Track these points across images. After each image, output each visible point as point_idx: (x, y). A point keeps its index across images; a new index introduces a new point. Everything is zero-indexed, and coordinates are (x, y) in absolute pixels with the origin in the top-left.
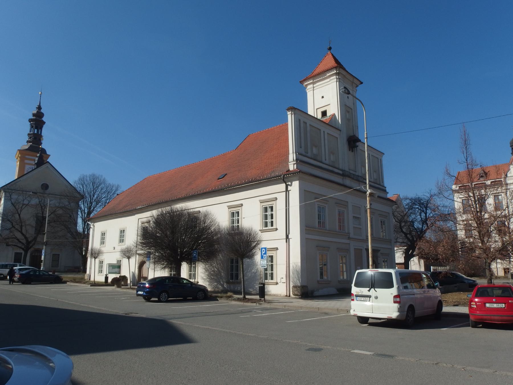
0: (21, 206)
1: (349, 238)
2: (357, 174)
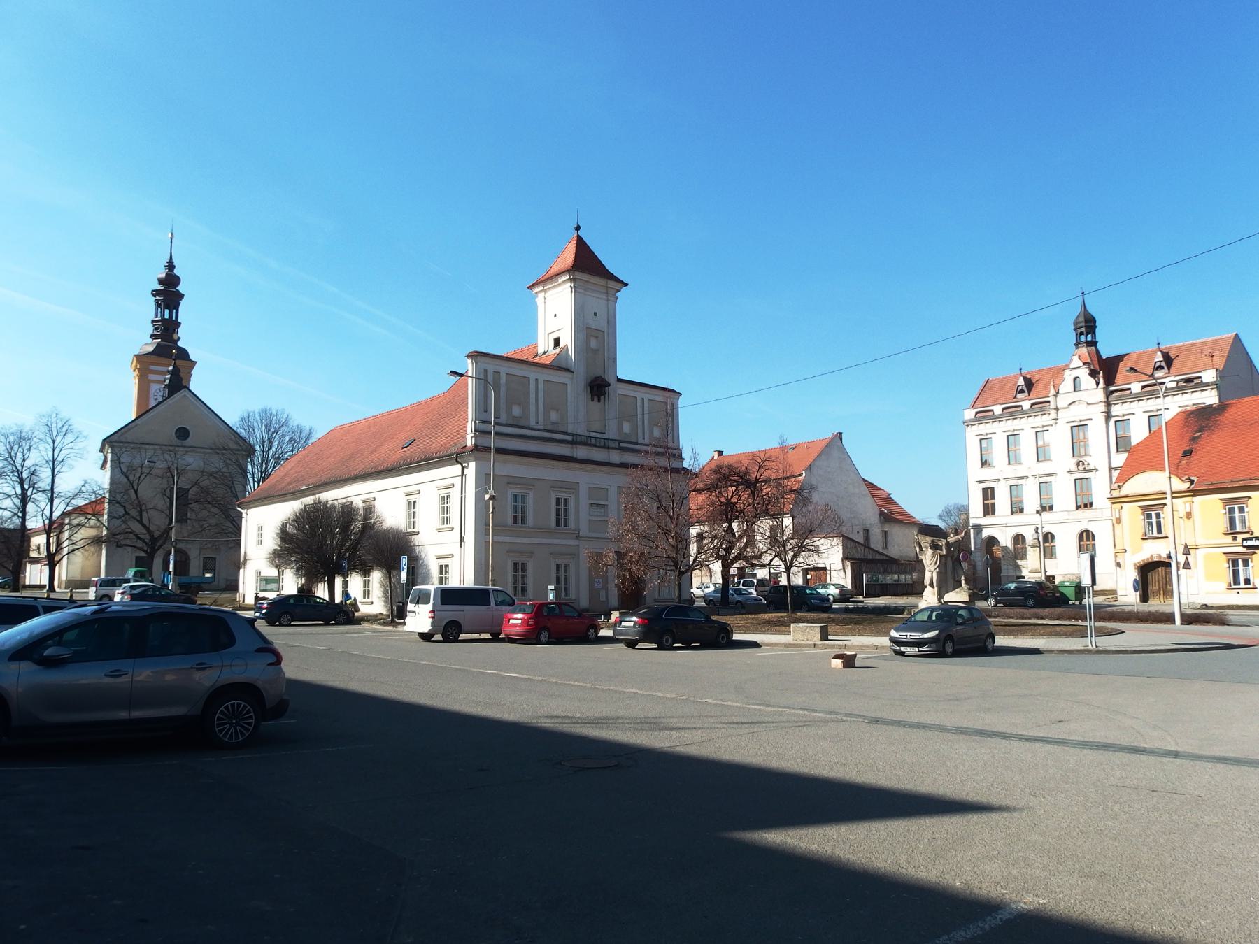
0: (138, 475)
1: (578, 537)
2: (606, 436)
